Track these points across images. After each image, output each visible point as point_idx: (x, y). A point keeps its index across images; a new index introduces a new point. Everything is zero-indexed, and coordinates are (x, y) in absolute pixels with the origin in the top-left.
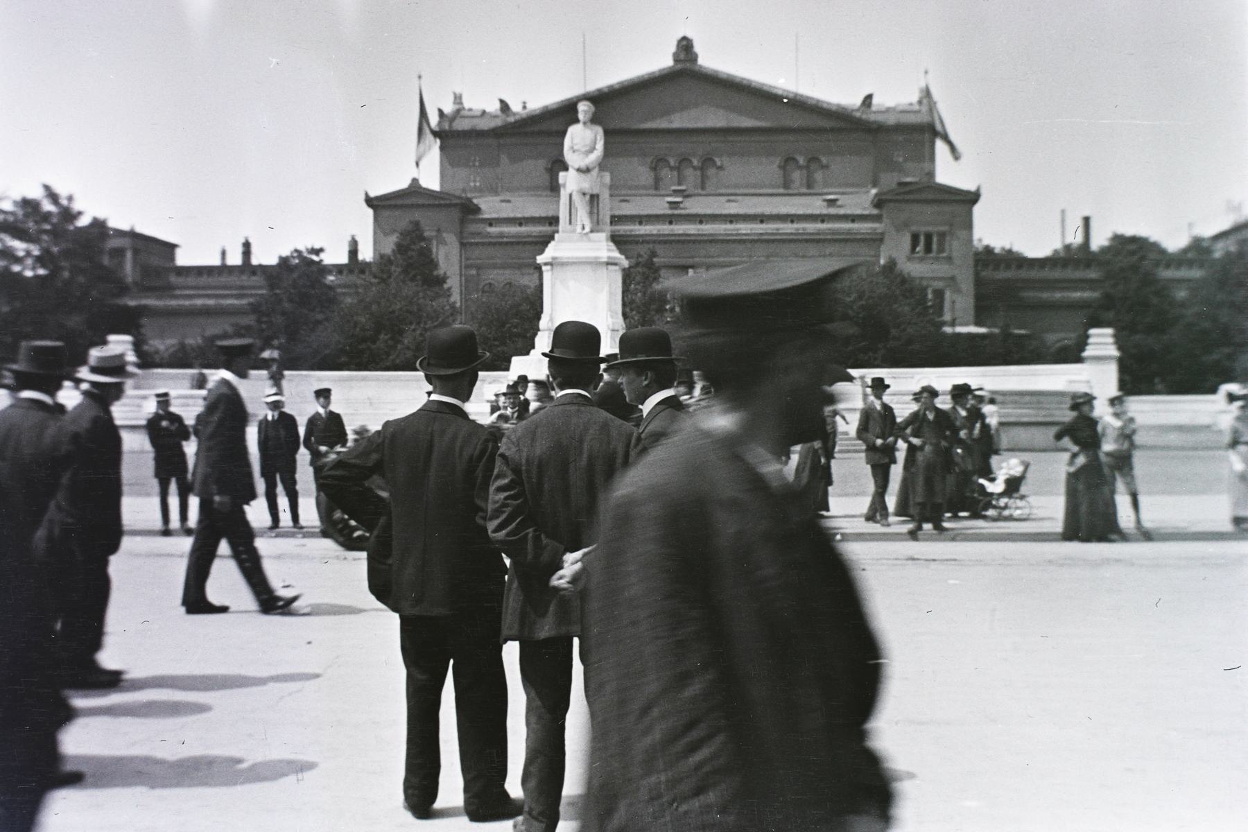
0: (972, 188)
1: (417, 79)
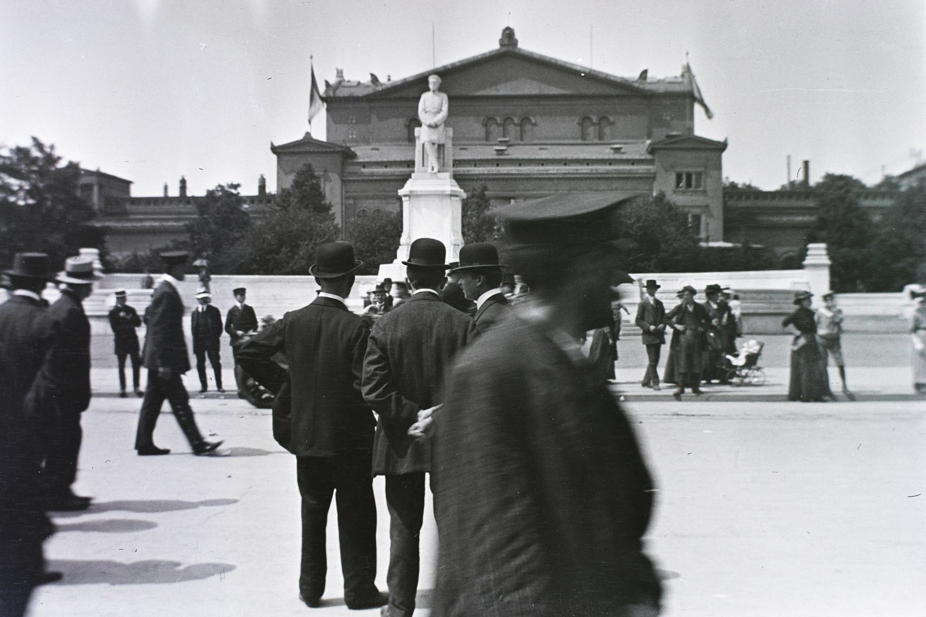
0: (722, 139)
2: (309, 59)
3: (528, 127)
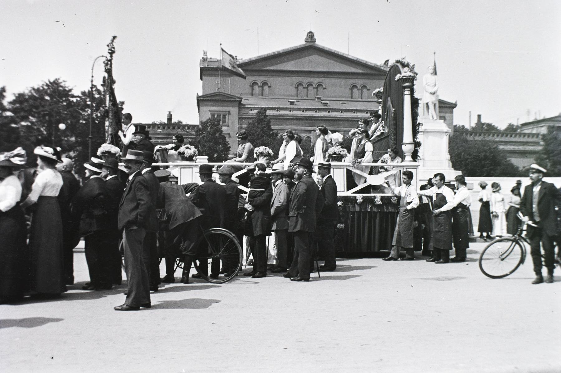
0: (454, 102)
1: (433, 54)
3: (320, 89)
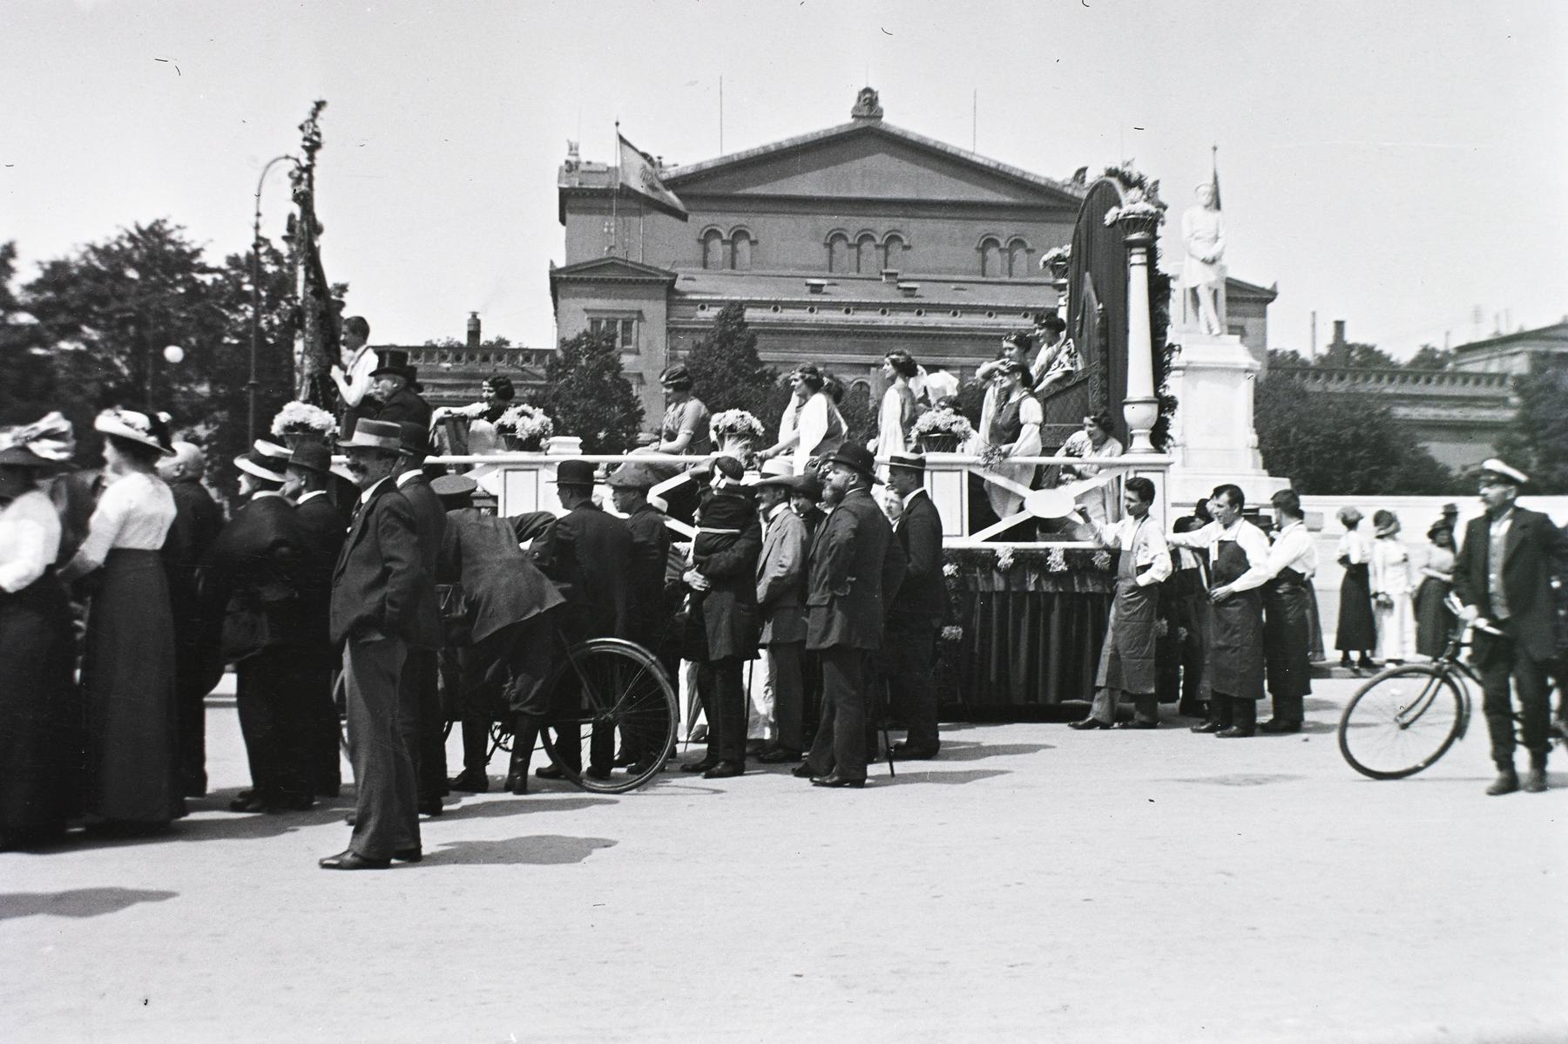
0: (1268, 286)
2: (1212, 151)
